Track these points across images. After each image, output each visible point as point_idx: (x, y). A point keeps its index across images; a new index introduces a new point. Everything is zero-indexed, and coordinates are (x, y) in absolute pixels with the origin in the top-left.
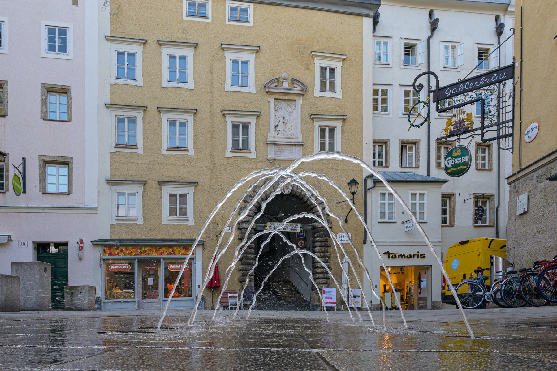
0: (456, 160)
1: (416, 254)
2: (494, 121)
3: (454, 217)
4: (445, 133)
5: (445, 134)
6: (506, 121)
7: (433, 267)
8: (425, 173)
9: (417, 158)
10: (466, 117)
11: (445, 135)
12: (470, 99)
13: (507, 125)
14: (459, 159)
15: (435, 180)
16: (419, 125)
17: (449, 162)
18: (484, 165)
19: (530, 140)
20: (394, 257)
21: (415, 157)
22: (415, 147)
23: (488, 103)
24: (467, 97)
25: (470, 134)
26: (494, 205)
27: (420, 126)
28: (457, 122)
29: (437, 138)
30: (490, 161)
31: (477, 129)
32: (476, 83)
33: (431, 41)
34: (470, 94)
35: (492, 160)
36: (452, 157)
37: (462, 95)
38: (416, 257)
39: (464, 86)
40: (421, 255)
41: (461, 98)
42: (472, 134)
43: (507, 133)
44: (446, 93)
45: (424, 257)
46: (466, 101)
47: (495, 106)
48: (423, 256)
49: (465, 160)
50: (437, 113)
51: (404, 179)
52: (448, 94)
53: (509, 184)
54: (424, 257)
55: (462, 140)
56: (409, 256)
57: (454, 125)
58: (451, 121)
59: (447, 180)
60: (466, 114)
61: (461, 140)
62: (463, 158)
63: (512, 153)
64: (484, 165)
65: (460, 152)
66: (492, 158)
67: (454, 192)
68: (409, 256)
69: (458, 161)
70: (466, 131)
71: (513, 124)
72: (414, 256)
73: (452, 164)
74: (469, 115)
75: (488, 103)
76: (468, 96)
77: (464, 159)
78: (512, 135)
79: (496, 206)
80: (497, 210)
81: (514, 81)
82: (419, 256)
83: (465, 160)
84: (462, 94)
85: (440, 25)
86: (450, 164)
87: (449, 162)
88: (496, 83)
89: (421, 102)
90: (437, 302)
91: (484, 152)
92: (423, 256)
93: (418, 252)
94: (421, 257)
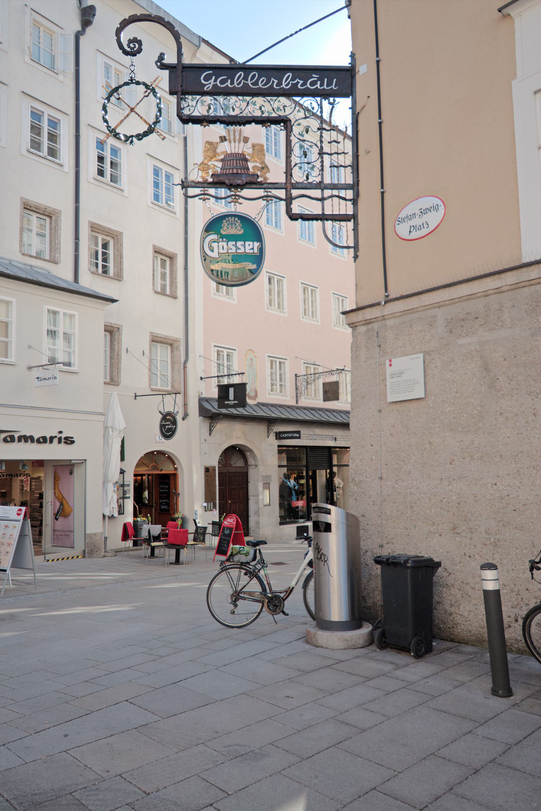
0: (231, 243)
1: (56, 437)
2: (315, 179)
3: (119, 369)
4: (200, 173)
5: (202, 177)
6: (345, 184)
7: (88, 462)
8: (69, 276)
9: (53, 245)
10: (250, 151)
11: (201, 180)
12: (258, 113)
13: (342, 193)
14: (239, 244)
15: (93, 294)
16: (132, 136)
17: (215, 245)
18: (164, 287)
19: (415, 235)
20: (9, 439)
21: (51, 241)
22: (51, 224)
23: (300, 134)
24: (250, 108)
25: (261, 192)
26: (180, 357)
27: (134, 139)
28: (228, 159)
29: (350, 108)
30: (173, 283)
31: (276, 186)
32: (273, 82)
33: (82, 39)
34: (259, 100)
35: (176, 283)
36: (222, 236)
37: (241, 98)
38: (56, 441)
39: (246, 78)
40: (66, 438)
41: (238, 104)
42: (265, 194)
43: (343, 212)
44: (203, 81)
45: (73, 442)
46: (250, 115)
47: (316, 145)
48: (69, 441)
49: (253, 249)
50: (176, 122)
51: (34, 279)
52: (209, 85)
53: (353, 326)
54: (73, 442)
55: (241, 200)
56: (41, 440)
57: (222, 160)
58: (216, 148)
59: (115, 298)
60: (249, 144)
61: (239, 201)
62: (247, 243)
63: (356, 257)
64: (164, 287)
65: (239, 228)
66: (176, 279)
67: (119, 323)
68: (41, 440)
69: (237, 248)
70: (253, 183)
71: (357, 195)
72: (52, 439)
73: (221, 251)
74: (259, 149)
75: (300, 134)
76: (254, 104)
77: (251, 247)
78: (354, 217)
79: (183, 359)
80: (185, 367)
81: (354, 102)
82: (63, 441)
83: (253, 249)
84: (240, 95)
85: (96, 20)
86: (216, 250)
87: (215, 245)
88: (318, 96)
89: (138, 83)
90: (95, 534)
91: (163, 266)
92: (69, 441)
93: (60, 432)
94: (65, 442)
